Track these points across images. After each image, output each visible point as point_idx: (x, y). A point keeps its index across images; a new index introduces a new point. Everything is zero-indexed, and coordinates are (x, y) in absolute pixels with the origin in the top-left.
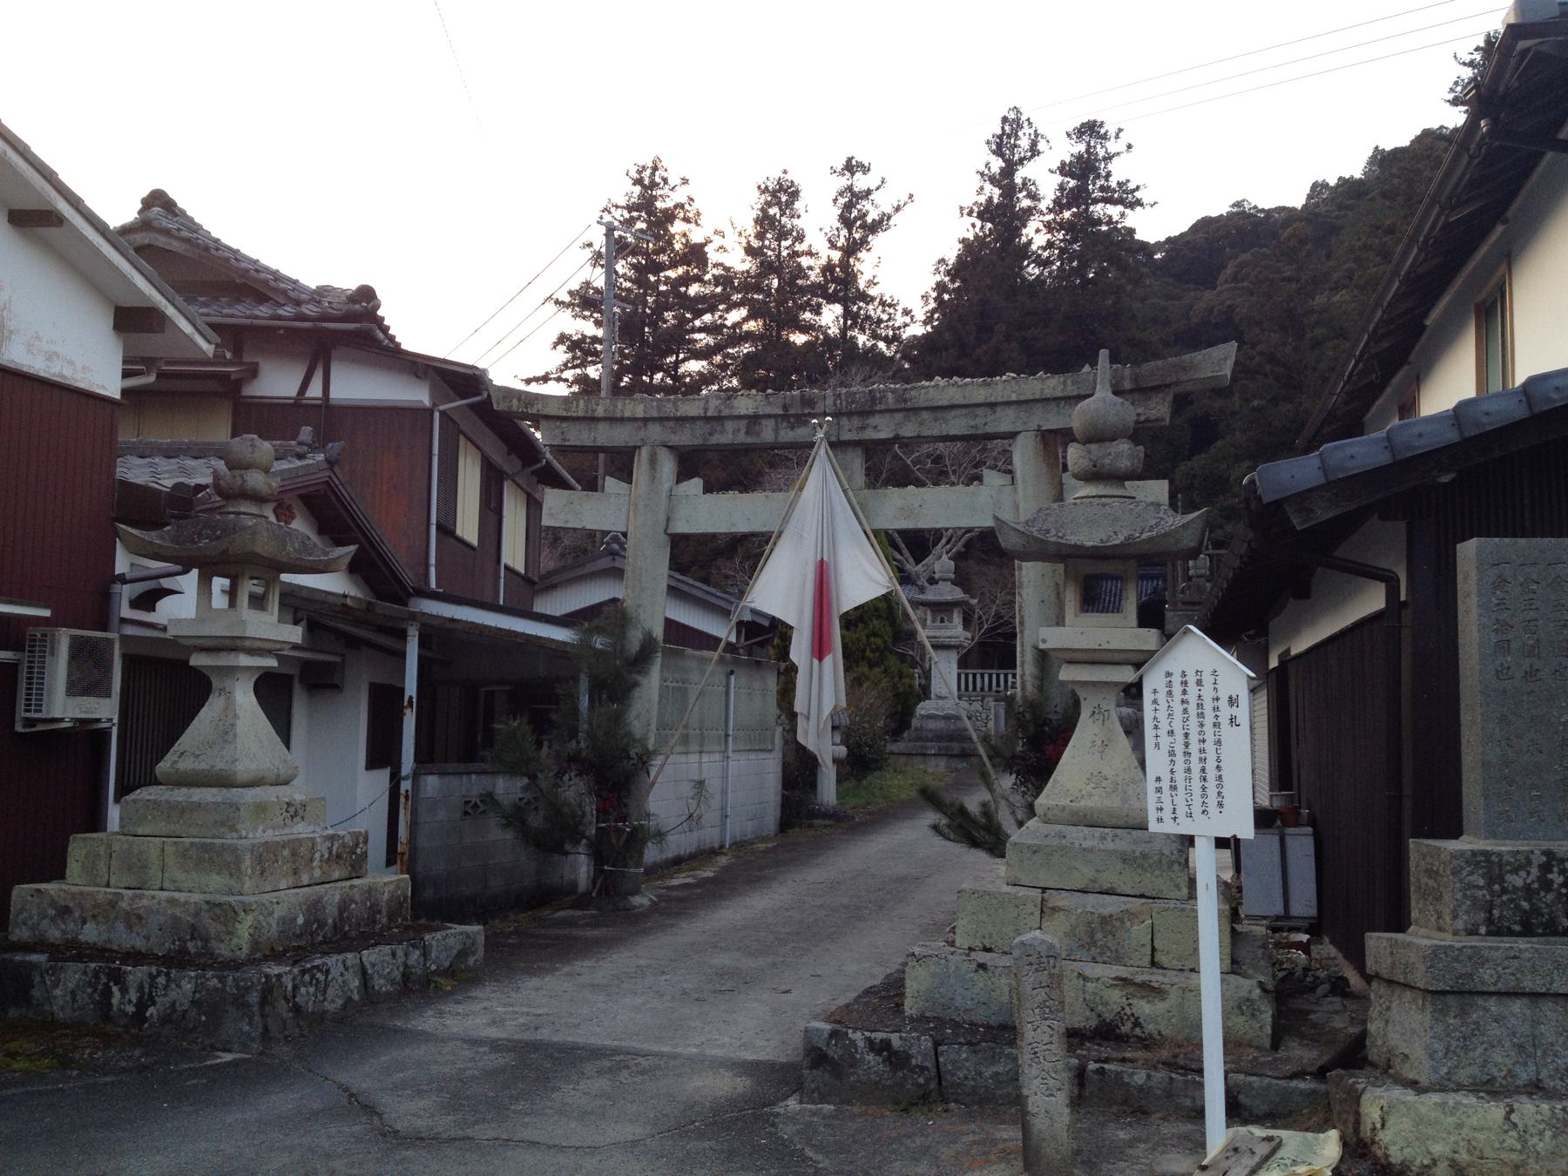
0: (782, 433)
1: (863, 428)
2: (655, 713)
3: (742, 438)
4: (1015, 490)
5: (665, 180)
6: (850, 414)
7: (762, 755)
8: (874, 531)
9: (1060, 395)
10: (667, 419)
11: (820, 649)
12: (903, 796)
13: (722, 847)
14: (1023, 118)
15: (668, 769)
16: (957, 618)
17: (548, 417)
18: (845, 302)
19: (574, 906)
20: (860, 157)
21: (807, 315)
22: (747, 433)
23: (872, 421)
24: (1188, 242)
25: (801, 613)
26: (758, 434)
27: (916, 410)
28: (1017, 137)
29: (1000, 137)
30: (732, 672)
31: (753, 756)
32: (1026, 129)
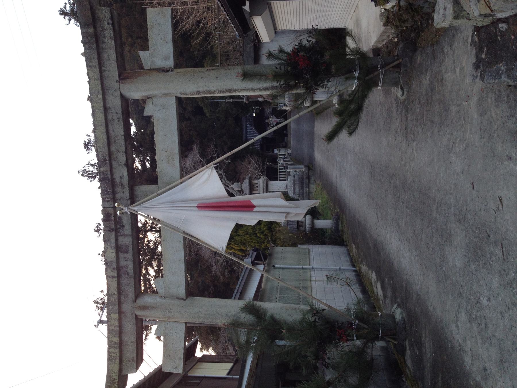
0: (126, 232)
1: (122, 185)
2: (288, 305)
3: (130, 256)
4: (155, 96)
5: (102, 299)
6: (114, 193)
7: (311, 253)
8: (181, 178)
9: (98, 69)
10: (119, 299)
11: (248, 207)
12: (326, 196)
13: (355, 271)
14: (83, 169)
15: (319, 297)
16: (256, 181)
17: (120, 370)
18: (146, 232)
19: (403, 355)
20: (94, 227)
21: (151, 244)
22: (127, 252)
23: (117, 180)
24: (136, 120)
25: (228, 219)
26: (127, 246)
27: (110, 154)
28: (89, 171)
29: (89, 177)
30: (274, 266)
31: (312, 257)
32: (86, 168)
